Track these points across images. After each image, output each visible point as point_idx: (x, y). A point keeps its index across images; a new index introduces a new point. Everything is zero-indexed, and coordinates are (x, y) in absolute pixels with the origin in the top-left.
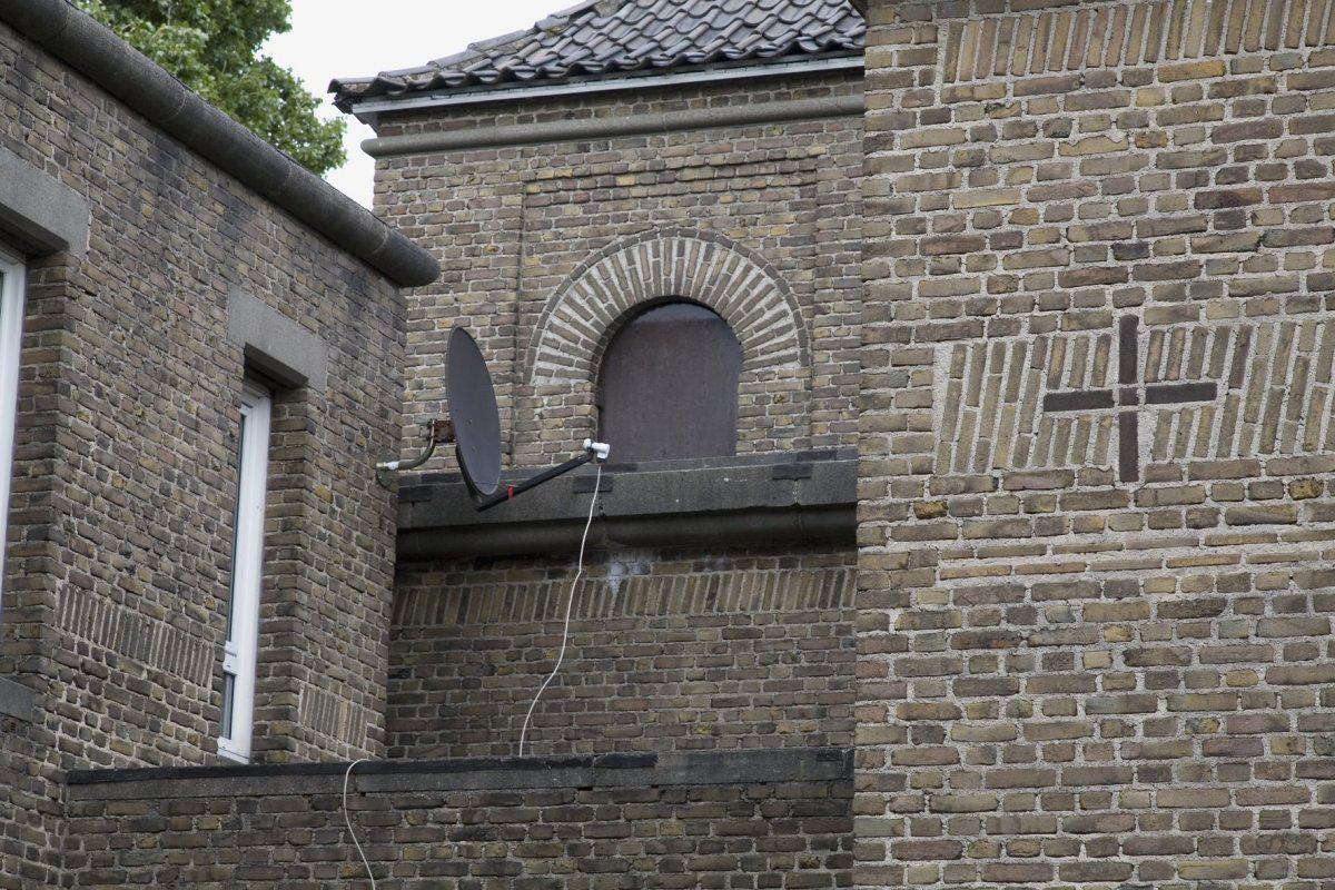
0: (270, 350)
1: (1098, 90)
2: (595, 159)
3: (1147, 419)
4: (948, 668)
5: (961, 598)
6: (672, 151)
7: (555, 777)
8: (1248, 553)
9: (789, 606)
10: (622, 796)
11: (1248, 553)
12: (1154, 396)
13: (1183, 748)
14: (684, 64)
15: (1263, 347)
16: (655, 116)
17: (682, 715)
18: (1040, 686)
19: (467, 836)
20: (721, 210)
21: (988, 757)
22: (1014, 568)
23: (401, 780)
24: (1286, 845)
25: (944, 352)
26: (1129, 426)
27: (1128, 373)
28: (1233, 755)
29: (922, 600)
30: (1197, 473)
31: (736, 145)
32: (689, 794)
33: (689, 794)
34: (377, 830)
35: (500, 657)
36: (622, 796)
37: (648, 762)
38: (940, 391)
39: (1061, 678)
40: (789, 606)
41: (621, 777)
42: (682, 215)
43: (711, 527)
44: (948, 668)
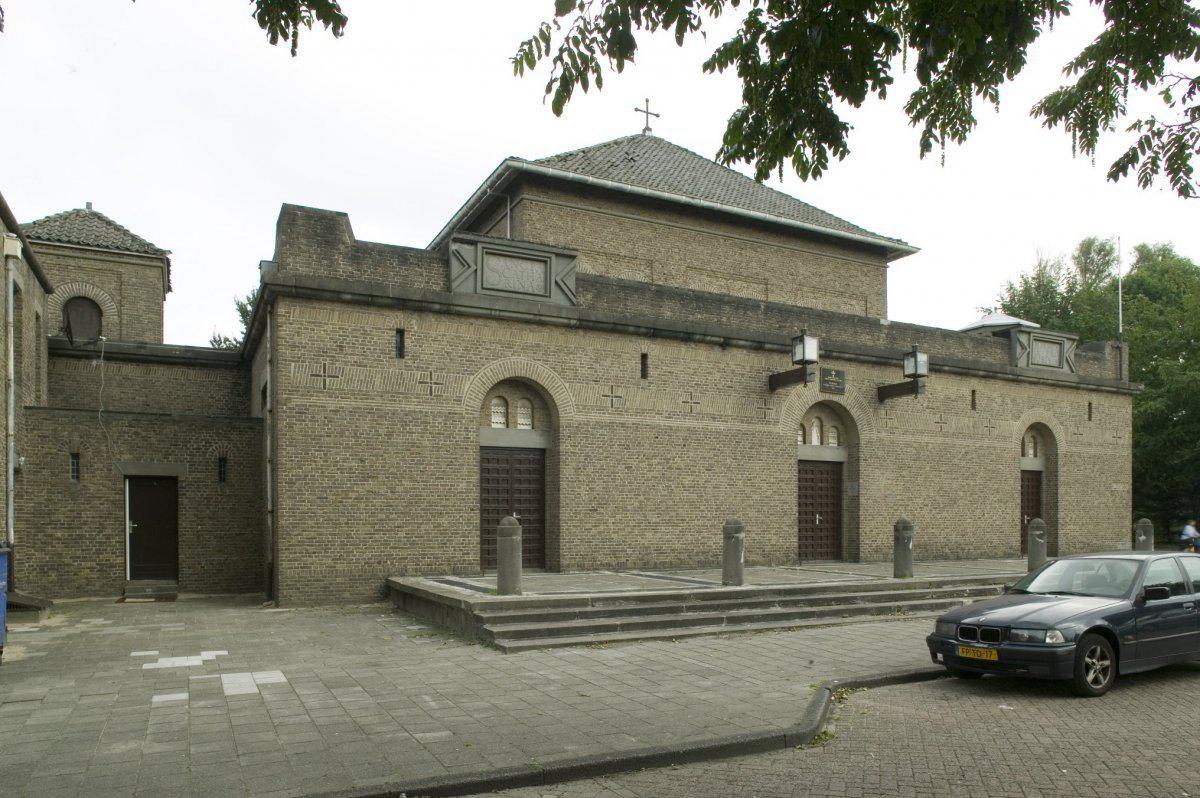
0: (567, 471)
1: (319, 324)
2: (61, 261)
3: (328, 380)
4: (294, 417)
5: (297, 405)
6: (83, 263)
7: (149, 417)
8: (343, 403)
9: (138, 374)
10: (164, 421)
11: (343, 403)
12: (330, 376)
13: (333, 432)
14: (88, 245)
15: (346, 371)
16: (77, 254)
17: (112, 395)
18: (310, 421)
19: (129, 426)
20: (97, 279)
21: (301, 431)
22: (304, 401)
23: (468, 491)
24: (349, 448)
25: (293, 364)
26: (325, 381)
27: (324, 372)
28: (341, 434)
29: (289, 405)
30: (336, 389)
31: (100, 265)
32: (178, 422)
33: (178, 422)
34: (107, 424)
35: (64, 377)
36: (164, 421)
37: (170, 415)
38: (292, 370)
39: (313, 420)
40: (138, 374)
41: (164, 418)
42: (86, 278)
43: (121, 356)
44: (294, 417)
